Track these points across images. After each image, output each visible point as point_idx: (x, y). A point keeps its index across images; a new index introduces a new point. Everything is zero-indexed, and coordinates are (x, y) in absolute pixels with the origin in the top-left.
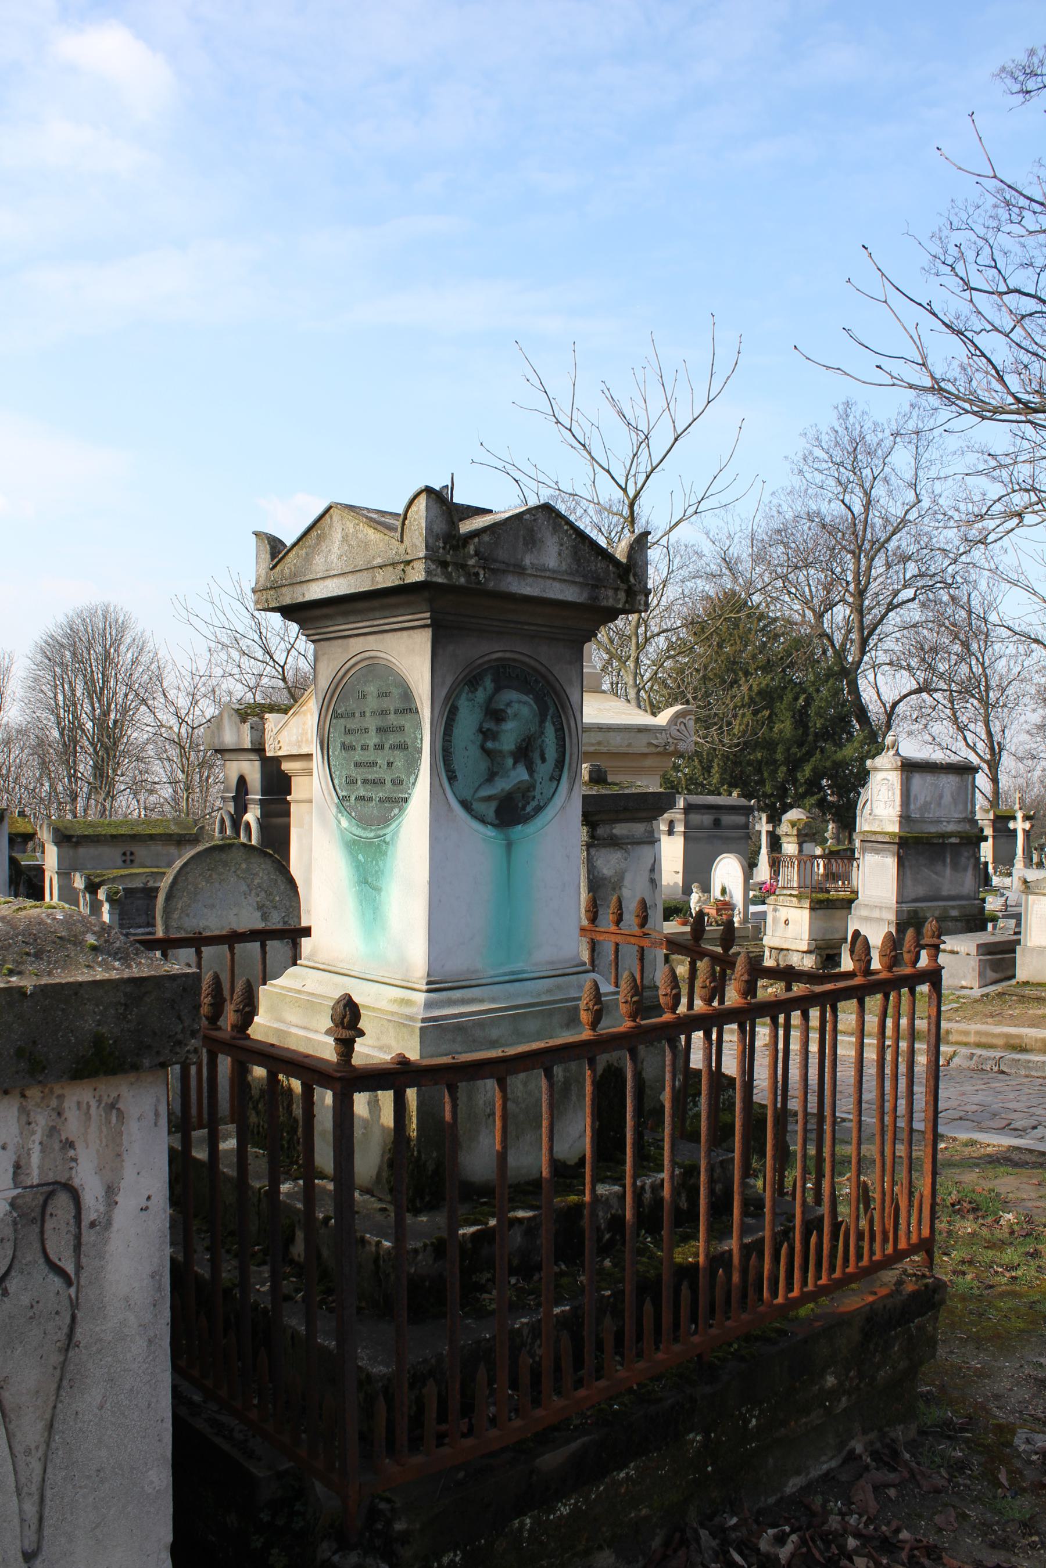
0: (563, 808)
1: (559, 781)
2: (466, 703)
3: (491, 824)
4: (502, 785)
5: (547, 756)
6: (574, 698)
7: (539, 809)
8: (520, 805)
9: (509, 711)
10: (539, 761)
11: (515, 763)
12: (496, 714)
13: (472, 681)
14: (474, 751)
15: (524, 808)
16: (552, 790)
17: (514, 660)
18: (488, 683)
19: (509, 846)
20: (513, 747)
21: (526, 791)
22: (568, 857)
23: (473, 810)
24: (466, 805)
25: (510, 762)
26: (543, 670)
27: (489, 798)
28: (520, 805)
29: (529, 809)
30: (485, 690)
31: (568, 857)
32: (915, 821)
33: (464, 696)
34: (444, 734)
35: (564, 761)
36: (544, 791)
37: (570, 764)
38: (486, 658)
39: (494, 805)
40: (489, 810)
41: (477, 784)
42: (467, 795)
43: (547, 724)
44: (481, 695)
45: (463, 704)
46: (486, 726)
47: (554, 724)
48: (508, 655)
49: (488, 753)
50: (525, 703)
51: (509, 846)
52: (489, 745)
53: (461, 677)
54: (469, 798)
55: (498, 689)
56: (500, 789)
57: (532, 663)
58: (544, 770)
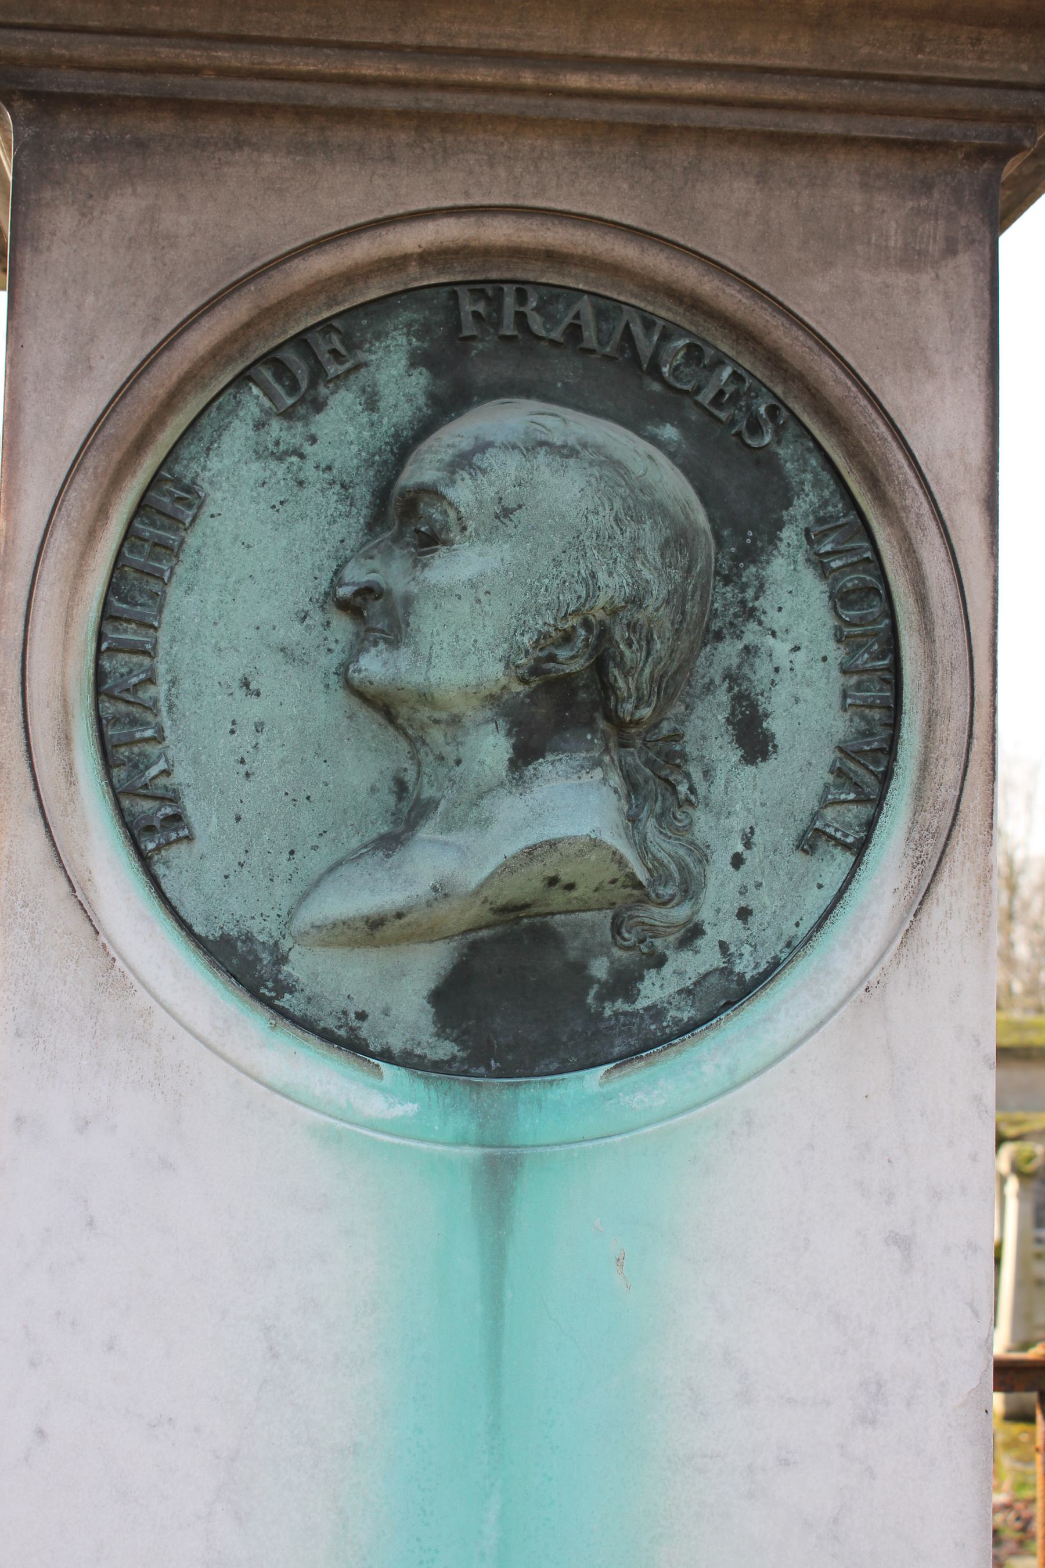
0: (867, 987)
1: (860, 849)
2: (255, 469)
3: (408, 1061)
4: (461, 862)
5: (776, 725)
6: (937, 428)
7: (731, 992)
8: (600, 968)
9: (462, 493)
10: (724, 753)
11: (525, 755)
12: (402, 516)
13: (292, 360)
14: (300, 702)
15: (625, 983)
16: (815, 901)
17: (552, 257)
18: (395, 375)
19: (499, 1172)
20: (494, 672)
21: (644, 905)
22: (902, 1242)
23: (284, 988)
24: (245, 966)
25: (492, 748)
26: (731, 299)
27: (374, 929)
28: (600, 968)
29: (655, 989)
30: (372, 403)
31: (902, 1242)
32: (195, 484)
33: (238, 436)
34: (107, 615)
35: (890, 750)
36: (763, 902)
37: (924, 767)
38: (362, 250)
39: (426, 965)
40: (402, 992)
41: (316, 863)
42: (246, 907)
43: (778, 568)
44: (343, 431)
45: (234, 473)
46: (357, 575)
47: (820, 565)
48: (499, 232)
49: (383, 706)
50: (567, 452)
51: (499, 1172)
52: (374, 666)
53: (200, 341)
54: (264, 930)
55: (448, 403)
56: (422, 889)
57: (660, 264)
58: (747, 802)
